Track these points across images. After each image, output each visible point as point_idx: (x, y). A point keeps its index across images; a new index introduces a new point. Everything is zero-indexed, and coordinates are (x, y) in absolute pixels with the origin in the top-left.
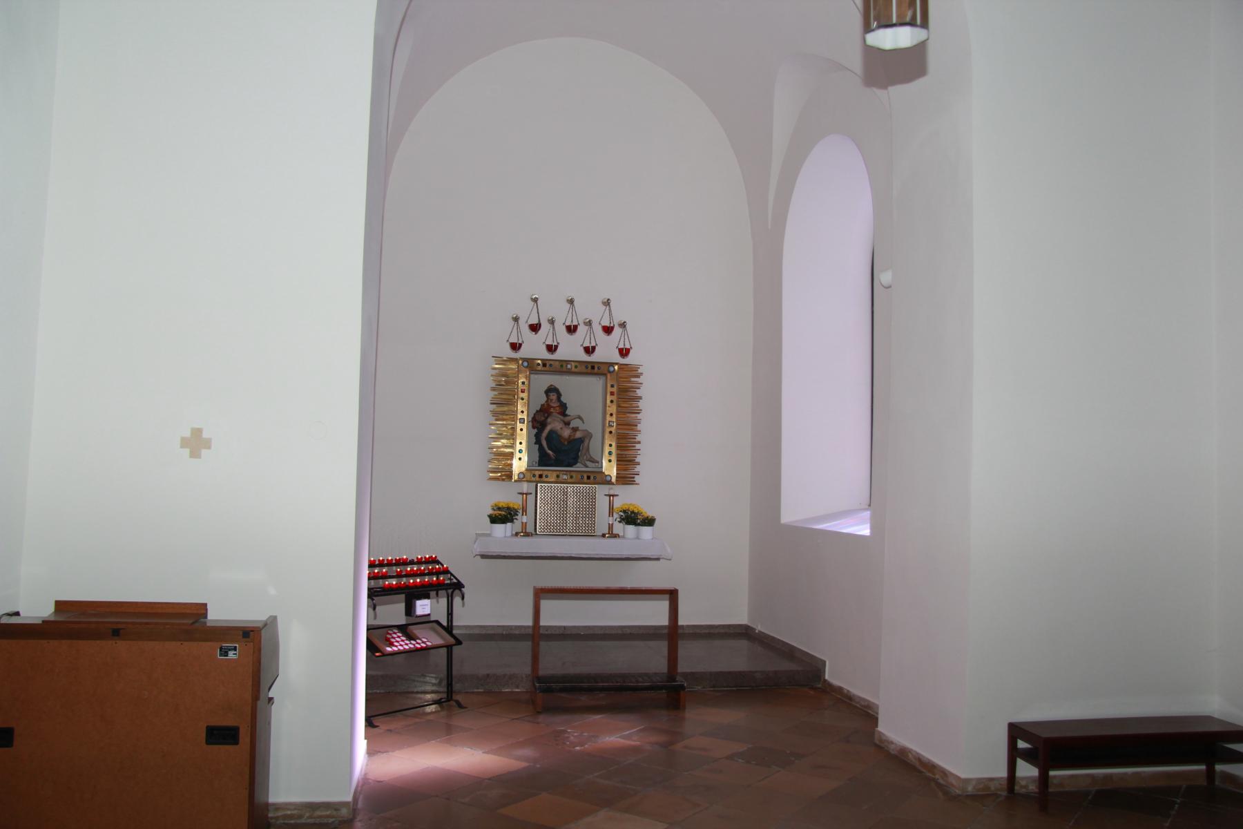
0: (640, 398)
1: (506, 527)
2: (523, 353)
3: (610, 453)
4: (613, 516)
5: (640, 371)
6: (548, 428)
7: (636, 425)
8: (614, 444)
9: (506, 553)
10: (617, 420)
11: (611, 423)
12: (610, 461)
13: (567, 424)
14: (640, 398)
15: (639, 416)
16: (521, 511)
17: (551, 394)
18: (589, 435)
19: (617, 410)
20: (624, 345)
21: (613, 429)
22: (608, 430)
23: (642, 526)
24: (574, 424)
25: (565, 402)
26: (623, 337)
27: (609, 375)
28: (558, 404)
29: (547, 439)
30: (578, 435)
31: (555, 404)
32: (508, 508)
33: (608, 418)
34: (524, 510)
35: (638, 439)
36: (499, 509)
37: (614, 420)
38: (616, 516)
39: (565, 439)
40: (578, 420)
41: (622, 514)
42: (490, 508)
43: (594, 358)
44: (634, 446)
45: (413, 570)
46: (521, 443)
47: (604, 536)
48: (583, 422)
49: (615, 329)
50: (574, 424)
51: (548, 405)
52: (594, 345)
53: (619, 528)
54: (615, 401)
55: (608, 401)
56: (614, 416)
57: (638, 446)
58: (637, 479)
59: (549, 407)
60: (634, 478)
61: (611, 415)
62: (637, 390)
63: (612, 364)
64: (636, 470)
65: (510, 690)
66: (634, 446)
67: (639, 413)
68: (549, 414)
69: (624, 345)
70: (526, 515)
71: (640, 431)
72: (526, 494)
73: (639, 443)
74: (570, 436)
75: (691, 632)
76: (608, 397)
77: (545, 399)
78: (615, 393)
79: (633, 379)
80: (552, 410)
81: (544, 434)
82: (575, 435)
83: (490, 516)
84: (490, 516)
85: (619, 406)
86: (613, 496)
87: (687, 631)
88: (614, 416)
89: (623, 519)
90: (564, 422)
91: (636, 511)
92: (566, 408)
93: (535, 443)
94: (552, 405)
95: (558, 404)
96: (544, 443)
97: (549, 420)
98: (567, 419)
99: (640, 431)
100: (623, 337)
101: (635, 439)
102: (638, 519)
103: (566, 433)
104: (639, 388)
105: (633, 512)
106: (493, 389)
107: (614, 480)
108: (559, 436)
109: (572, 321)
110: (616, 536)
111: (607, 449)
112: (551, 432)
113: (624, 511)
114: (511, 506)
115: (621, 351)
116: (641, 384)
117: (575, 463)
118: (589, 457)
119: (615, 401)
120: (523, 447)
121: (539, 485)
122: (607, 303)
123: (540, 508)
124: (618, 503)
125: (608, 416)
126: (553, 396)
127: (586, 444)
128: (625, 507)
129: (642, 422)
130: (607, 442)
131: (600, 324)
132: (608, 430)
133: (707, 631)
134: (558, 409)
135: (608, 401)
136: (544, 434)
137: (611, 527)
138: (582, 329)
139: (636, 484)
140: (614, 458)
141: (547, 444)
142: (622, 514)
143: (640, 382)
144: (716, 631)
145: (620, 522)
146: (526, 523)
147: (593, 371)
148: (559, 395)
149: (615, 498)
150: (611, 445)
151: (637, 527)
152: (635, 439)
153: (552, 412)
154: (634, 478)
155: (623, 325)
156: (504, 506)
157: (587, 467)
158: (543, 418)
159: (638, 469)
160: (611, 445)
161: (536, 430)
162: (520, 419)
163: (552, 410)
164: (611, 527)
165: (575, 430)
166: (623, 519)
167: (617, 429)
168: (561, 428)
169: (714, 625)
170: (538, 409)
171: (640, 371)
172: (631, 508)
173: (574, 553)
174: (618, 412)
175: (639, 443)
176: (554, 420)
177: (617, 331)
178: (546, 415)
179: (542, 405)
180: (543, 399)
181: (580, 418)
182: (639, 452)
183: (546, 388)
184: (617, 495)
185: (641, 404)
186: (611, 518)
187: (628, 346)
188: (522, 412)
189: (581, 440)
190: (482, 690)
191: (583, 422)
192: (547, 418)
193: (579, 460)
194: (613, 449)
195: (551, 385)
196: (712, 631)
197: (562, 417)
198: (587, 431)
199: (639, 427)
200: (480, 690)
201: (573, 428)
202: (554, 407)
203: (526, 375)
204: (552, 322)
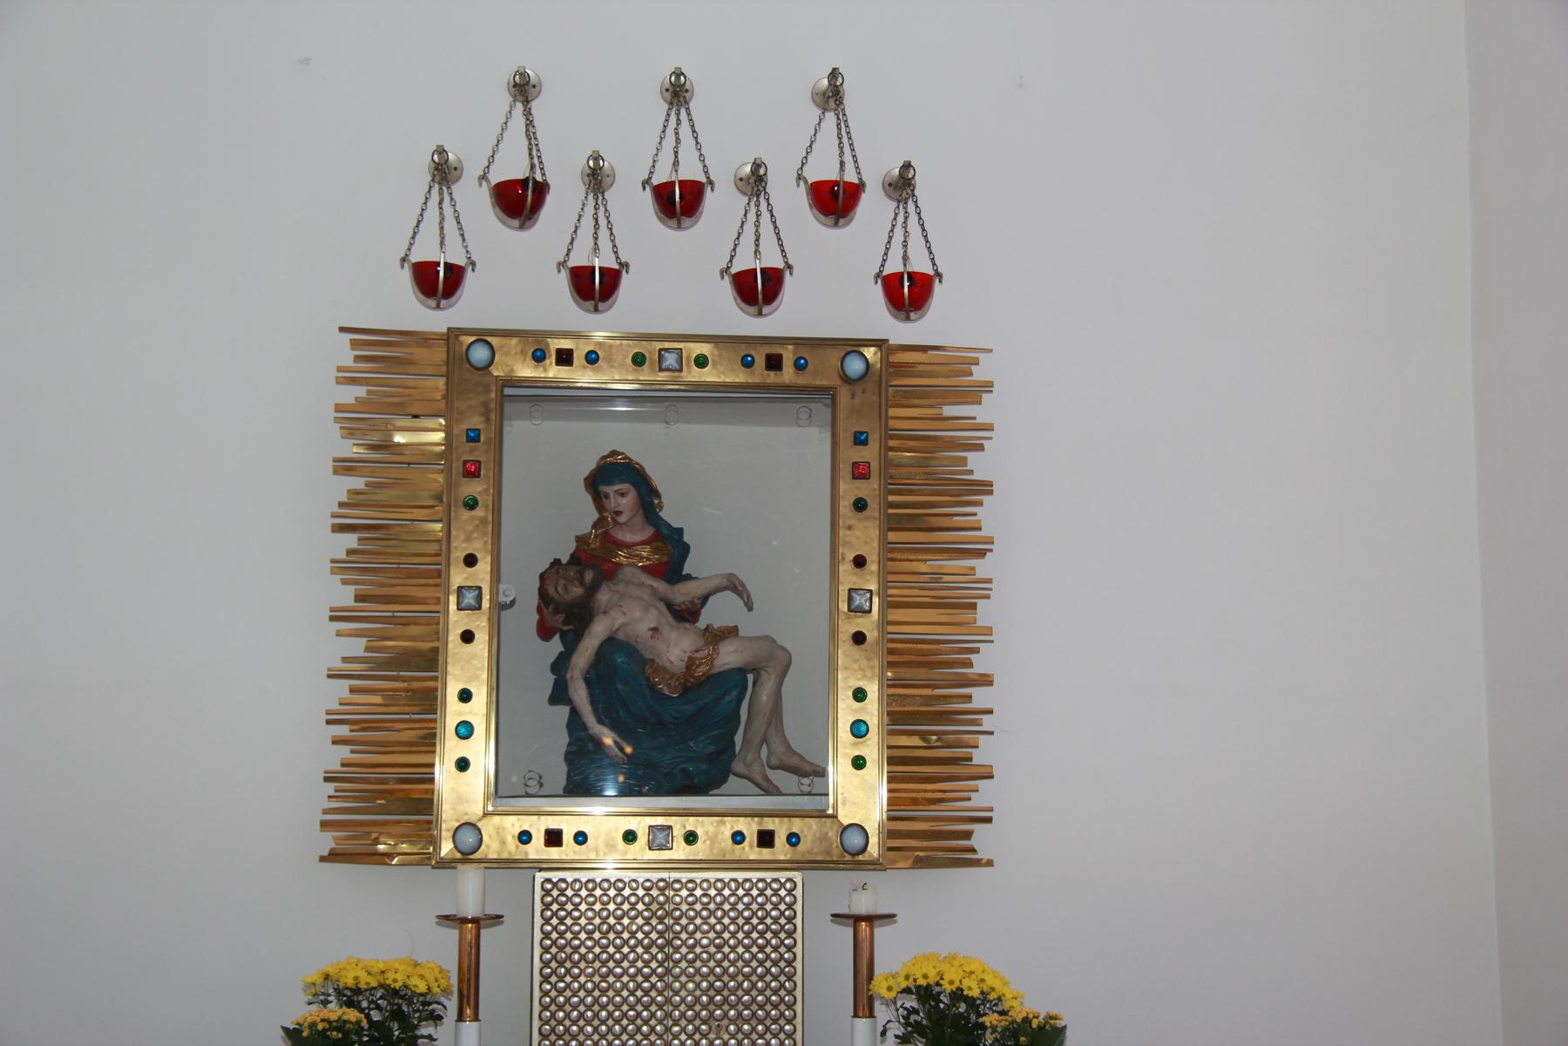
0: (985, 488)
2: (465, 311)
3: (859, 730)
4: (871, 1015)
5: (979, 374)
6: (598, 631)
7: (973, 606)
8: (872, 690)
10: (884, 585)
11: (859, 600)
12: (859, 763)
13: (686, 614)
14: (985, 488)
15: (982, 567)
16: (452, 1005)
17: (610, 490)
19: (883, 539)
20: (905, 258)
21: (868, 625)
24: (720, 611)
26: (899, 232)
27: (844, 395)
28: (649, 532)
29: (598, 676)
30: (729, 656)
31: (635, 533)
32: (392, 993)
35: (980, 664)
36: (350, 996)
37: (873, 587)
38: (882, 1013)
40: (729, 595)
42: (302, 993)
44: (969, 698)
46: (465, 696)
48: (750, 608)
49: (865, 198)
51: (606, 538)
52: (779, 264)
54: (873, 505)
56: (872, 566)
58: (983, 840)
59: (610, 543)
60: (968, 835)
61: (860, 562)
63: (853, 346)
64: (977, 800)
67: (981, 554)
68: (609, 573)
69: (905, 258)
70: (476, 1018)
71: (988, 631)
72: (475, 921)
73: (985, 681)
74: (691, 663)
76: (844, 486)
78: (874, 466)
79: (949, 411)
82: (711, 660)
85: (892, 523)
86: (871, 919)
88: (872, 566)
90: (669, 606)
91: (975, 993)
92: (685, 549)
94: (628, 537)
95: (649, 532)
98: (683, 593)
100: (899, 232)
102: (983, 1027)
103: (676, 649)
104: (980, 448)
105: (958, 995)
107: (874, 849)
109: (676, 163)
111: (847, 711)
112: (611, 644)
113: (926, 994)
114: (397, 979)
116: (989, 428)
117: (723, 780)
118: (779, 749)
119: (873, 505)
120: (477, 711)
122: (832, 96)
125: (846, 567)
126: (623, 499)
127: (768, 685)
128: (925, 973)
129: (996, 591)
130: (847, 682)
131: (800, 177)
132: (848, 628)
134: (645, 552)
135: (845, 504)
138: (722, 205)
139: (977, 863)
140: (871, 749)
141: (594, 702)
142: (911, 1002)
143: (981, 419)
150: (859, 695)
153: (619, 565)
155: (902, 186)
157: (776, 791)
158: (577, 591)
159: (984, 795)
160: (859, 695)
163: (621, 557)
165: (717, 636)
167: (884, 622)
168: (655, 630)
171: (979, 374)
172: (952, 978)
174: (889, 552)
175: (985, 681)
177: (874, 207)
178: (589, 576)
179: (581, 540)
180: (585, 516)
181: (734, 585)
182: (987, 722)
183: (591, 465)
184: (890, 917)
185: (990, 515)
186: (862, 1024)
187: (921, 265)
188: (525, 837)
189: (737, 678)
191: (750, 608)
192: (592, 590)
193: (738, 766)
194: (871, 711)
195: (614, 453)
197: (661, 586)
198: (770, 640)
199: (985, 613)
202: (629, 546)
203: (485, 404)
204: (597, 179)
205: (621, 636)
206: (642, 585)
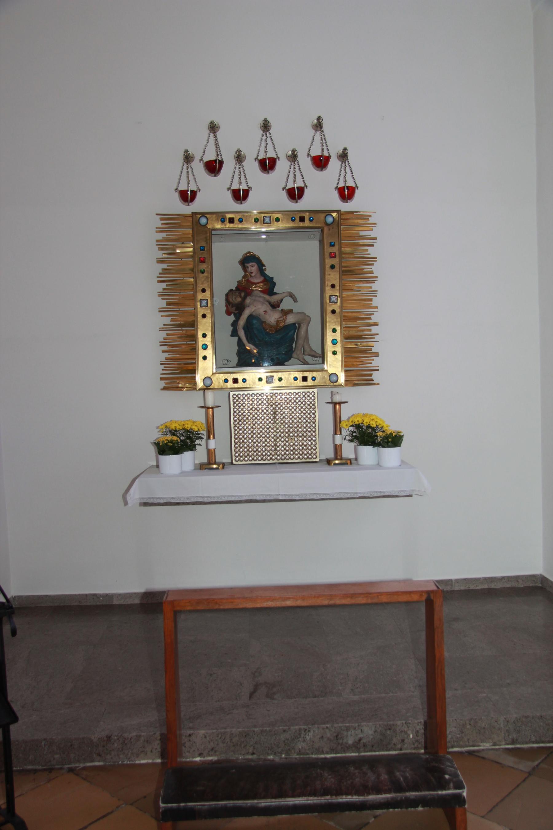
1: (181, 458)
4: (341, 434)
7: (371, 300)
9: (179, 498)
17: (249, 265)
18: (307, 319)
21: (336, 307)
22: (329, 308)
23: (383, 447)
24: (287, 304)
25: (271, 276)
28: (262, 279)
29: (248, 327)
30: (290, 319)
31: (258, 279)
33: (329, 291)
34: (210, 431)
35: (374, 319)
36: (174, 432)
39: (271, 326)
41: (351, 429)
43: (304, 204)
44: (370, 330)
45: (372, 434)
47: (329, 462)
49: (331, 161)
50: (287, 304)
51: (248, 281)
52: (302, 185)
53: (349, 449)
55: (327, 267)
57: (374, 330)
58: (375, 376)
60: (371, 375)
61: (333, 286)
62: (370, 249)
63: (328, 212)
64: (374, 364)
65: (150, 761)
66: (374, 338)
67: (373, 282)
69: (345, 181)
70: (214, 438)
72: (212, 408)
73: (376, 324)
74: (278, 322)
75: (462, 588)
77: (243, 274)
80: (253, 287)
81: (242, 322)
82: (284, 320)
83: (157, 444)
84: (157, 444)
86: (340, 403)
87: (457, 588)
89: (356, 437)
90: (270, 303)
91: (374, 426)
92: (274, 284)
93: (232, 335)
95: (262, 279)
96: (242, 333)
97: (248, 301)
98: (274, 299)
99: (376, 308)
101: (370, 319)
102: (377, 436)
103: (272, 318)
105: (369, 427)
106: (160, 261)
108: (263, 323)
110: (347, 462)
112: (251, 317)
115: (341, 191)
116: (375, 239)
119: (337, 267)
121: (232, 393)
123: (235, 426)
124: (346, 412)
125: (328, 289)
126: (253, 268)
127: (302, 332)
133: (486, 586)
134: (261, 285)
136: (242, 322)
137: (337, 449)
138: (282, 165)
139: (374, 384)
144: (499, 586)
145: (351, 441)
146: (215, 449)
147: (327, 255)
148: (261, 265)
149: (342, 405)
151: (376, 448)
152: (370, 319)
153: (253, 290)
154: (163, 224)
155: (344, 156)
156: (178, 427)
158: (239, 299)
159: (376, 362)
160: (334, 331)
161: (232, 318)
162: (201, 301)
163: (253, 287)
164: (337, 449)
165: (286, 313)
166: (356, 437)
169: (495, 578)
170: (234, 286)
171: (371, 220)
172: (366, 421)
173: (282, 493)
175: (376, 324)
176: (255, 300)
177: (334, 164)
178: (243, 294)
179: (239, 282)
180: (240, 274)
181: (291, 295)
185: (376, 268)
189: (294, 327)
190: (101, 763)
192: (244, 298)
194: (338, 336)
196: (493, 586)
197: (267, 297)
198: (304, 314)
200: (97, 764)
201: (282, 310)
202: (256, 284)
204: (239, 158)
205: (254, 314)
206: (260, 297)
